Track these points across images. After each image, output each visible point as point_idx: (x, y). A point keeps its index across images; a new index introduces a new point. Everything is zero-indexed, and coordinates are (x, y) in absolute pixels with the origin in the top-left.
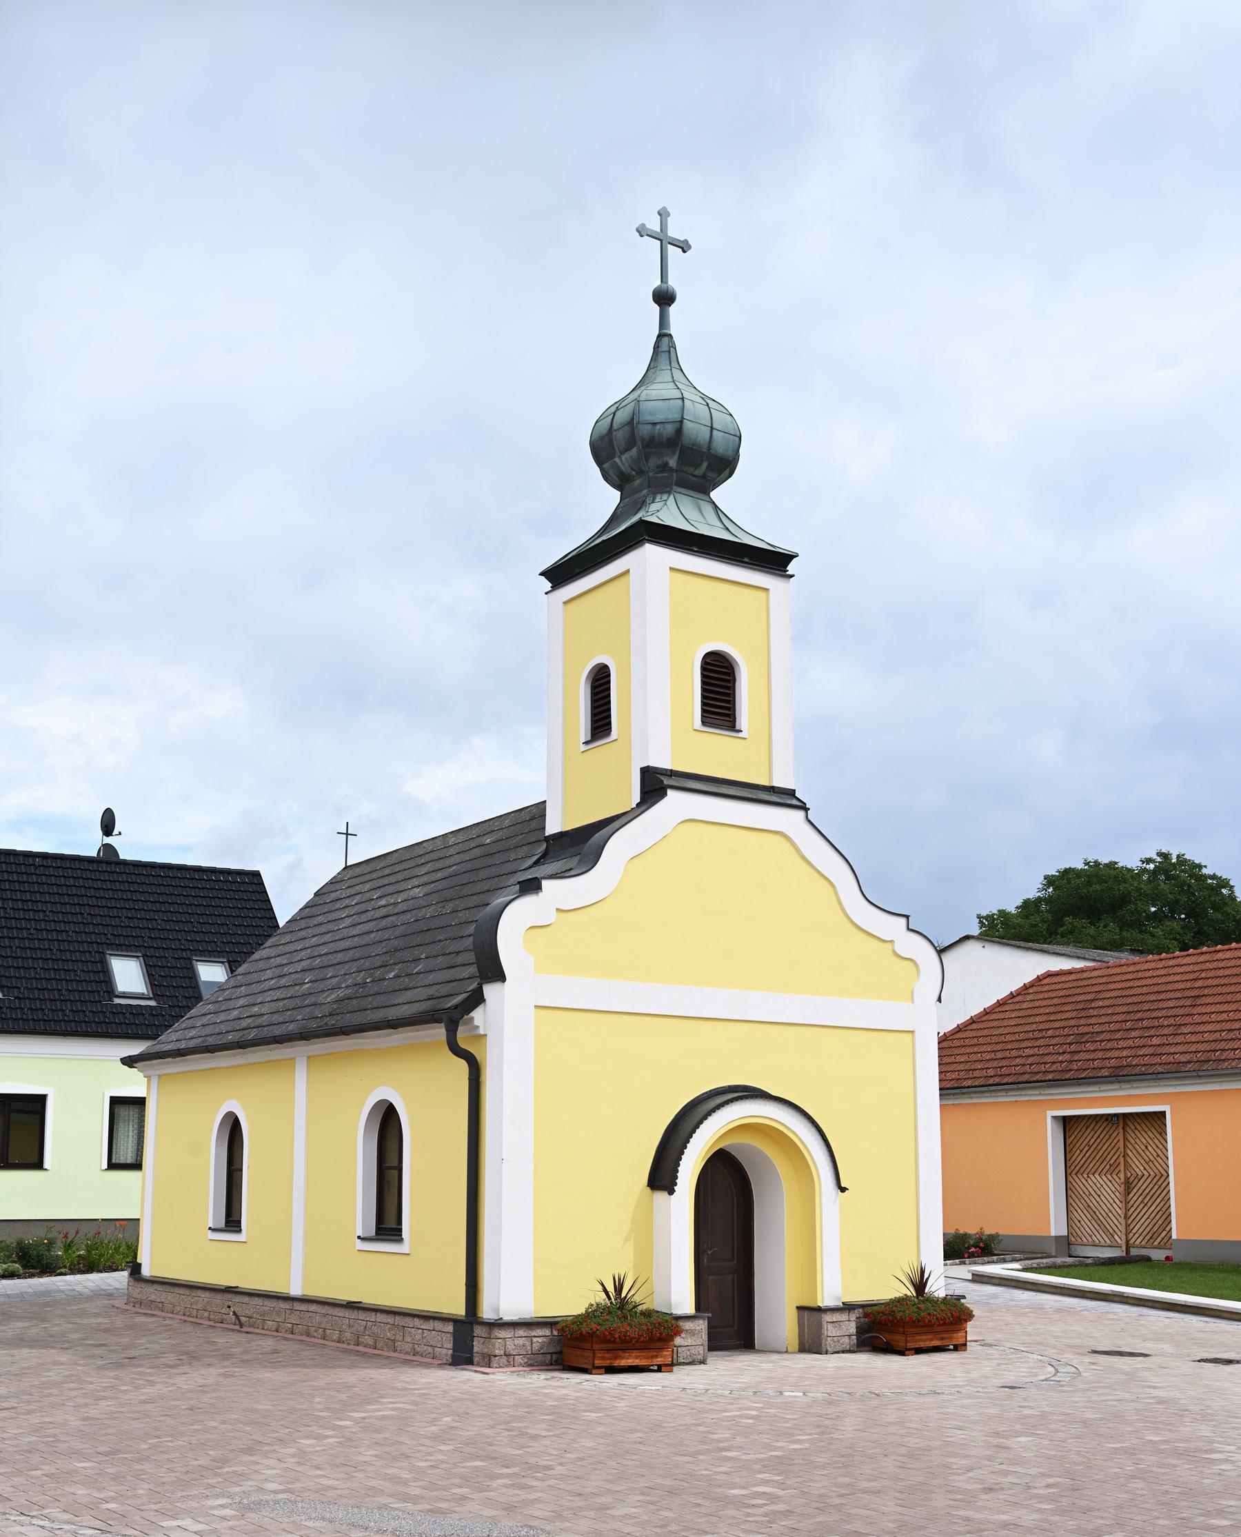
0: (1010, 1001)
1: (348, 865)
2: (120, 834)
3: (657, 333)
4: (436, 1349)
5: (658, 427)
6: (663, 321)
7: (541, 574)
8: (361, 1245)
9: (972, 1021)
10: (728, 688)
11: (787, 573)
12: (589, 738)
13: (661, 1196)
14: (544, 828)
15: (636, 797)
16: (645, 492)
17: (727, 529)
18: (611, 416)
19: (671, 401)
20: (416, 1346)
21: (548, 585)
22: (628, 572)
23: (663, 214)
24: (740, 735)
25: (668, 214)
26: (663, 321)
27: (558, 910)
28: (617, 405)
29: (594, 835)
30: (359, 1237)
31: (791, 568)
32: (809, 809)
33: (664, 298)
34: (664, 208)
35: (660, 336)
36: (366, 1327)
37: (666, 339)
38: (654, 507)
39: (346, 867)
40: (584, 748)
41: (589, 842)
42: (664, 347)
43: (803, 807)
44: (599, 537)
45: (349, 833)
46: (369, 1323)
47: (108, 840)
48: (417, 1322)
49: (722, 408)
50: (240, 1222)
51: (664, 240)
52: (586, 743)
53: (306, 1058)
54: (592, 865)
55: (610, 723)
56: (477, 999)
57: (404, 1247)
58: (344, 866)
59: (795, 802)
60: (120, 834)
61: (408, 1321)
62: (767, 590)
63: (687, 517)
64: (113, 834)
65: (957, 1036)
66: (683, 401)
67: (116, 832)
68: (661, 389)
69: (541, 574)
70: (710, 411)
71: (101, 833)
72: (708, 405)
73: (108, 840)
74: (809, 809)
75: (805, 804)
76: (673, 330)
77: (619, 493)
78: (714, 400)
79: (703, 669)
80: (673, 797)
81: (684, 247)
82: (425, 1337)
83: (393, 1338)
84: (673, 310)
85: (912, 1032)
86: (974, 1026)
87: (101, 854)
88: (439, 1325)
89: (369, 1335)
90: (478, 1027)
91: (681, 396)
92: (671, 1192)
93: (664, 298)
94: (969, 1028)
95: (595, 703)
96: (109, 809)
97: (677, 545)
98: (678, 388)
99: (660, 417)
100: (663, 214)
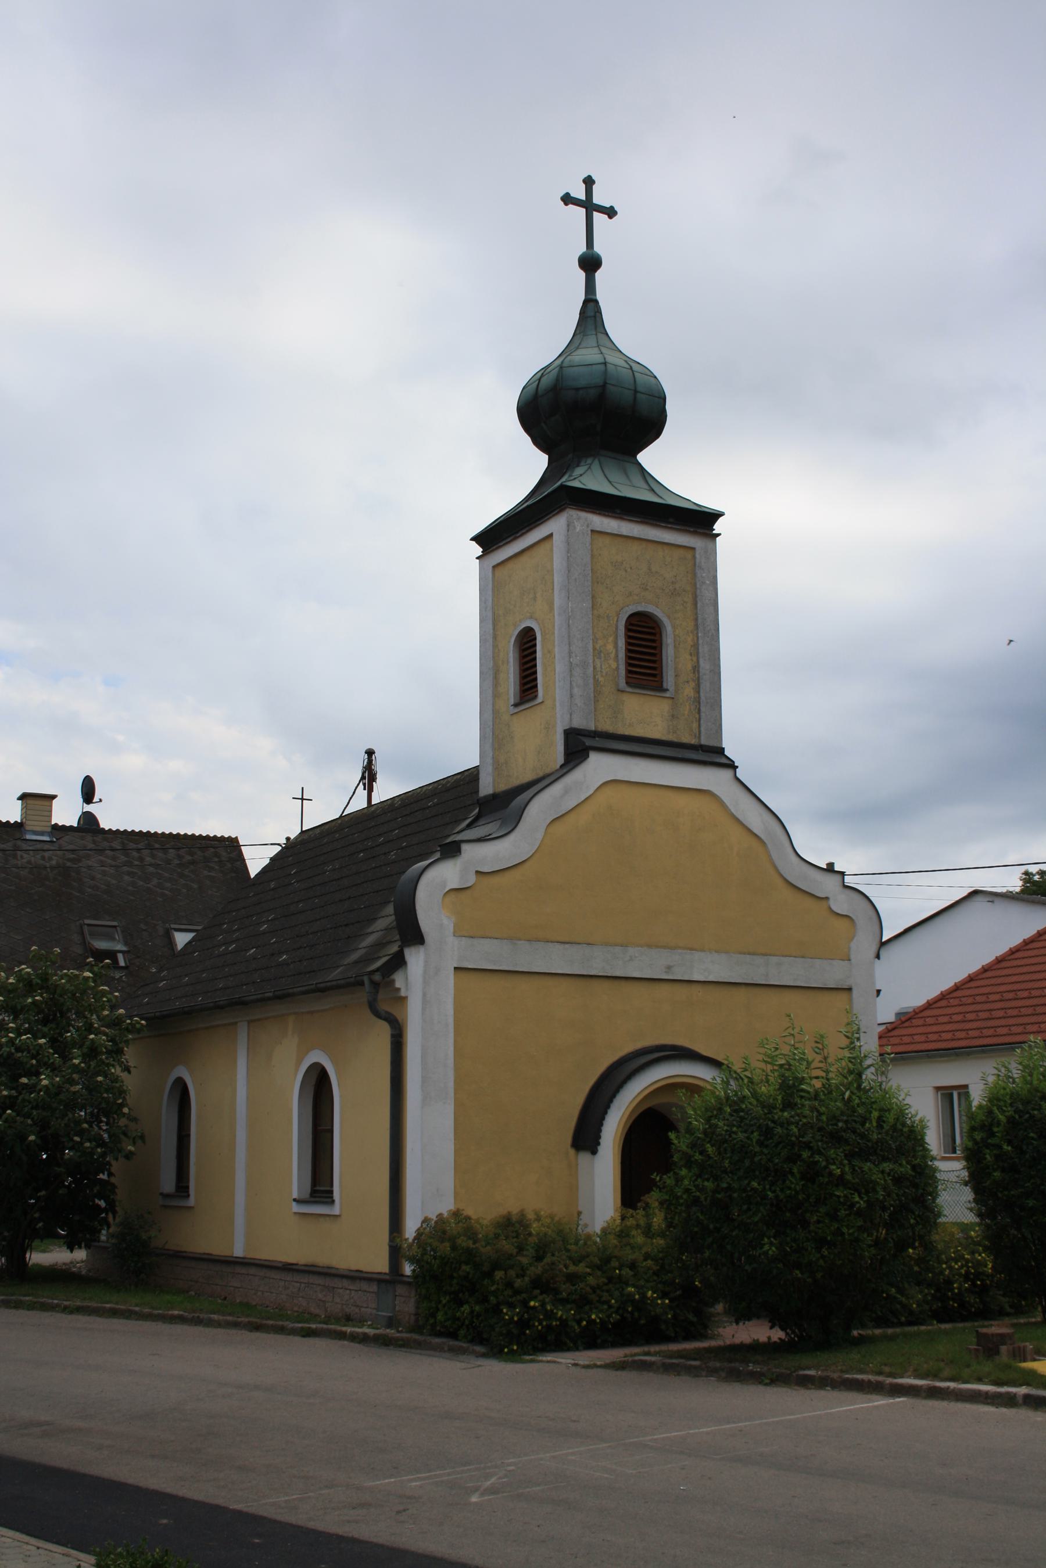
0: (1010, 958)
1: (304, 829)
2: (101, 800)
3: (582, 297)
4: (363, 1309)
5: (581, 392)
6: (590, 286)
7: (472, 539)
8: (296, 1208)
9: (971, 979)
10: (654, 648)
11: (714, 532)
12: (518, 700)
13: (584, 1157)
14: (478, 791)
15: (560, 759)
16: (570, 456)
17: (653, 490)
18: (537, 382)
19: (594, 366)
20: (344, 1307)
21: (479, 550)
22: (551, 536)
23: (589, 182)
24: (667, 695)
25: (593, 182)
26: (590, 286)
27: (477, 872)
28: (542, 371)
29: (516, 797)
30: (295, 1200)
31: (718, 527)
32: (737, 767)
33: (590, 263)
34: (589, 177)
35: (586, 302)
36: (300, 1289)
37: (591, 305)
38: (578, 471)
39: (302, 832)
40: (513, 710)
41: (510, 806)
42: (590, 312)
43: (731, 766)
44: (527, 501)
45: (304, 797)
46: (303, 1285)
47: (89, 808)
48: (346, 1283)
49: (646, 370)
50: (188, 1187)
51: (589, 206)
52: (516, 705)
53: (246, 1024)
54: (514, 825)
55: (536, 686)
56: (398, 962)
57: (336, 1210)
58: (300, 831)
59: (724, 761)
60: (101, 800)
61: (337, 1283)
62: (693, 549)
63: (611, 480)
64: (94, 801)
65: (954, 995)
66: (606, 365)
67: (96, 799)
68: (588, 355)
69: (472, 539)
70: (633, 374)
71: (82, 800)
72: (631, 368)
73: (89, 808)
74: (737, 767)
75: (734, 762)
76: (600, 296)
77: (546, 457)
78: (639, 363)
79: (628, 629)
80: (594, 758)
81: (611, 212)
82: (353, 1298)
83: (324, 1299)
84: (599, 275)
85: (850, 989)
86: (972, 984)
87: (82, 823)
88: (364, 1286)
89: (302, 1297)
90: (399, 989)
91: (603, 361)
92: (594, 1152)
93: (590, 263)
94: (967, 986)
95: (523, 666)
96: (88, 776)
97: (502, 518)
98: (602, 353)
99: (582, 383)
100: (589, 182)
